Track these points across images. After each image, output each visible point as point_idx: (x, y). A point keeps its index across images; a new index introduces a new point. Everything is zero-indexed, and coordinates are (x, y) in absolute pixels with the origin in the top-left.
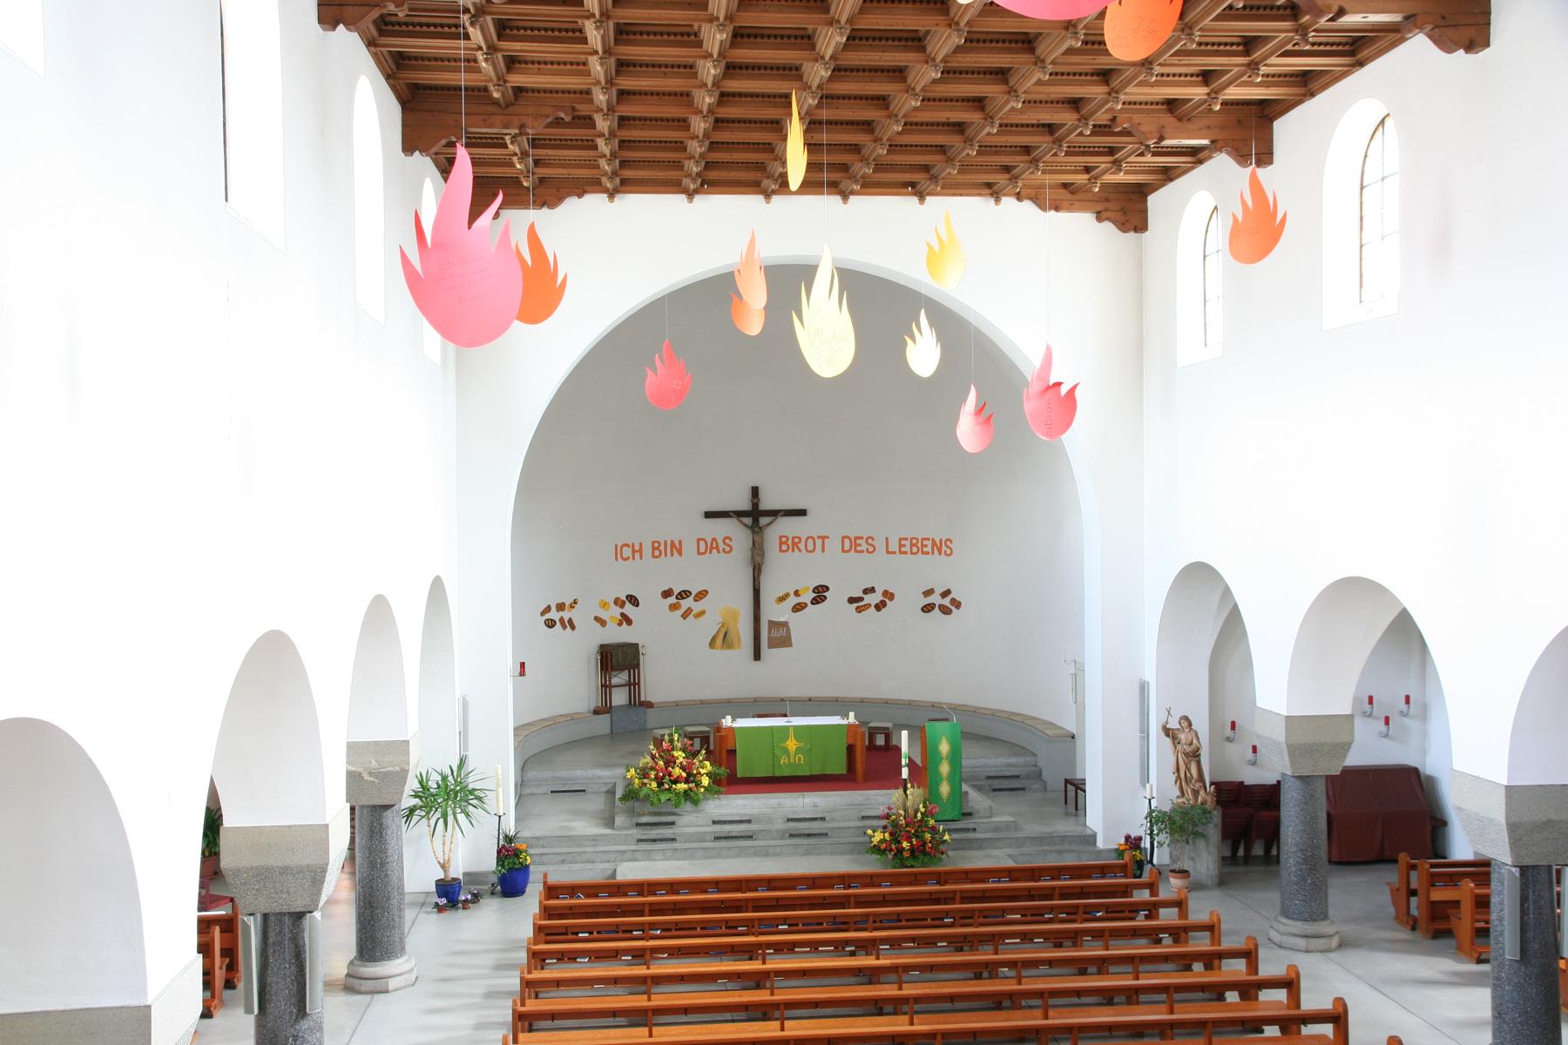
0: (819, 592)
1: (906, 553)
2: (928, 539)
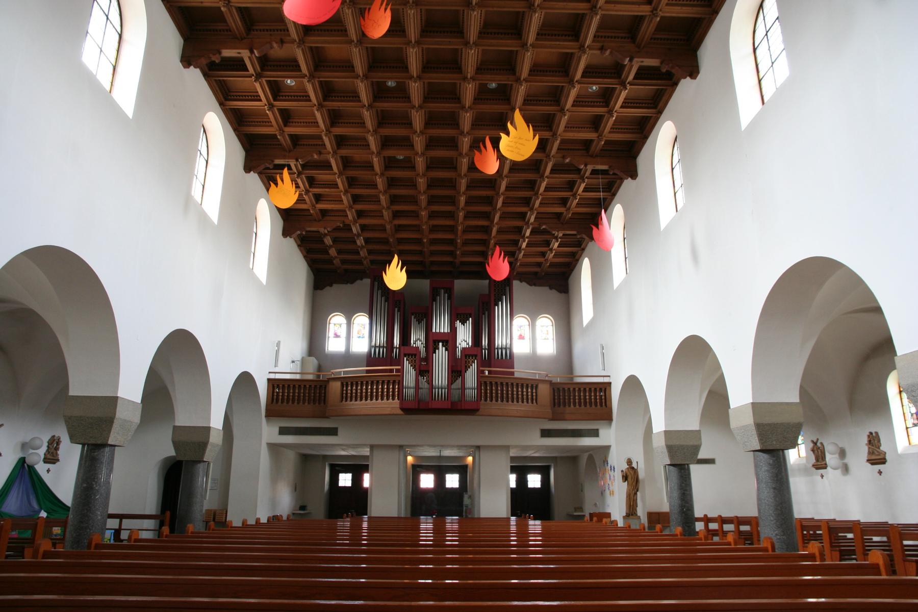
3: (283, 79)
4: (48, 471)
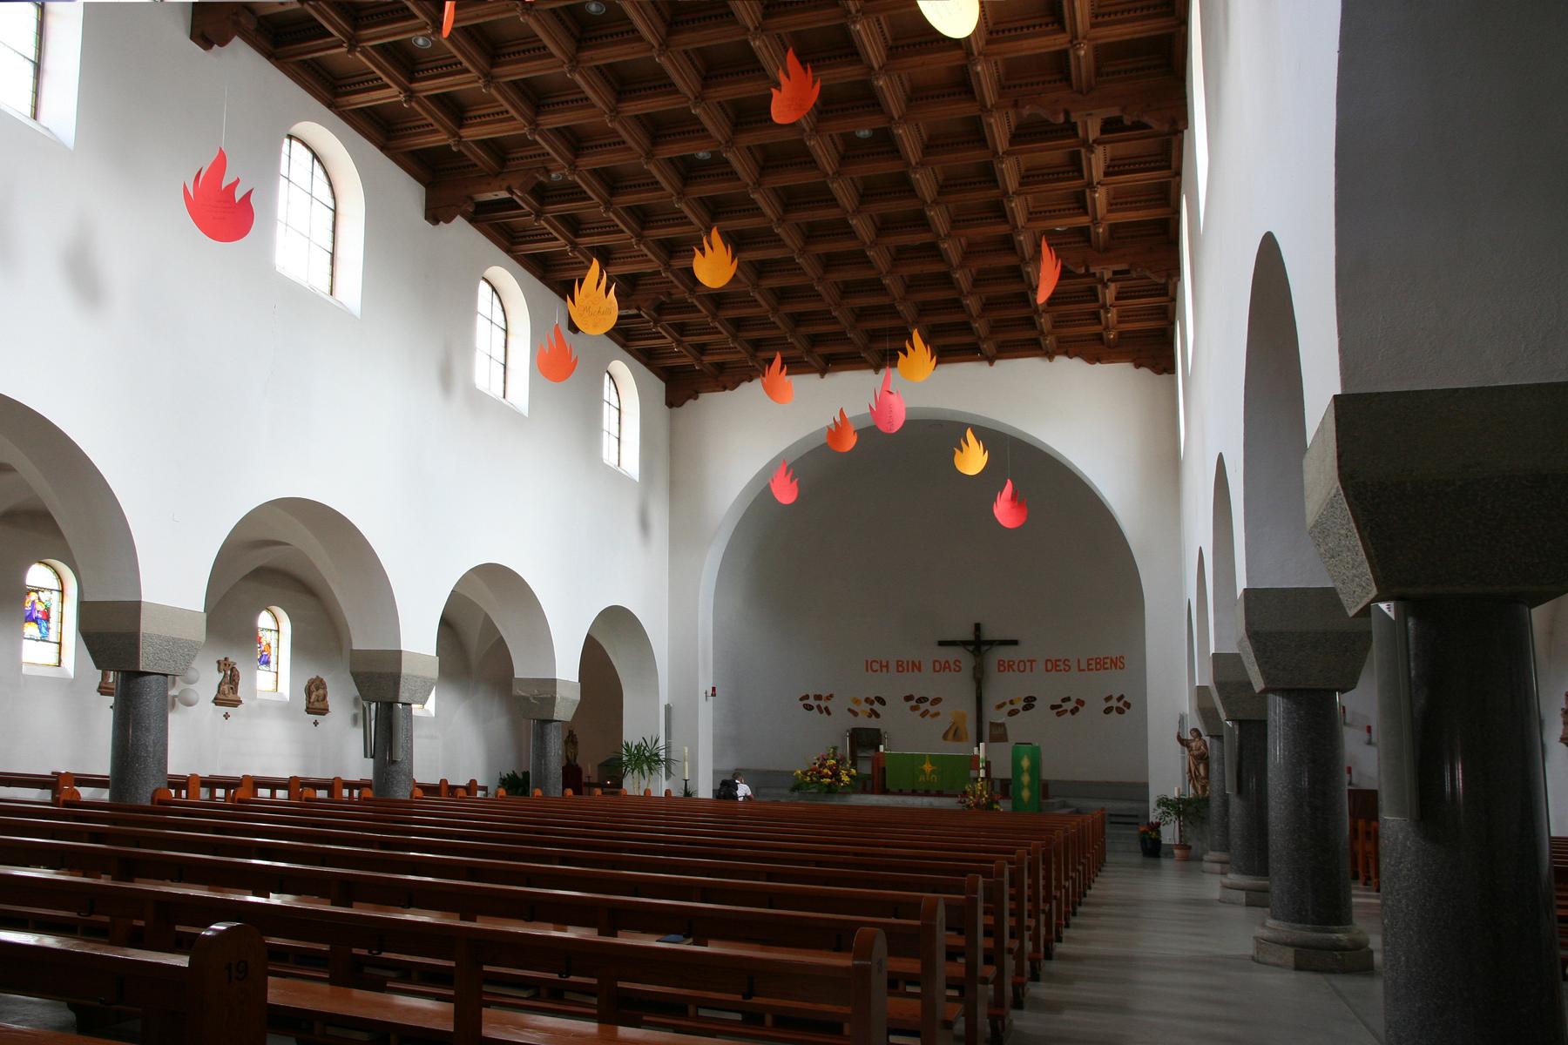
0: (1028, 701)
1: (1092, 669)
2: (1107, 658)
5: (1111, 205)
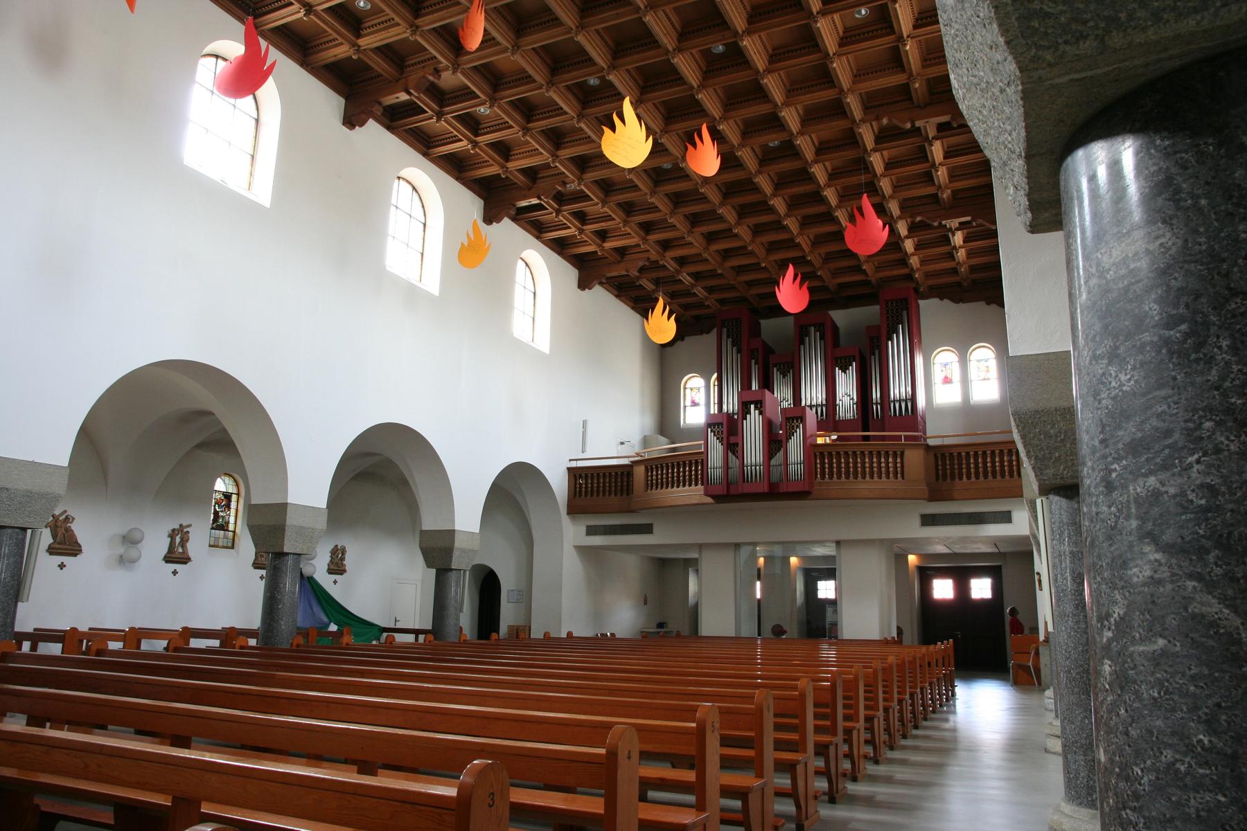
3: (474, 109)
4: (335, 582)
5: (926, 60)
